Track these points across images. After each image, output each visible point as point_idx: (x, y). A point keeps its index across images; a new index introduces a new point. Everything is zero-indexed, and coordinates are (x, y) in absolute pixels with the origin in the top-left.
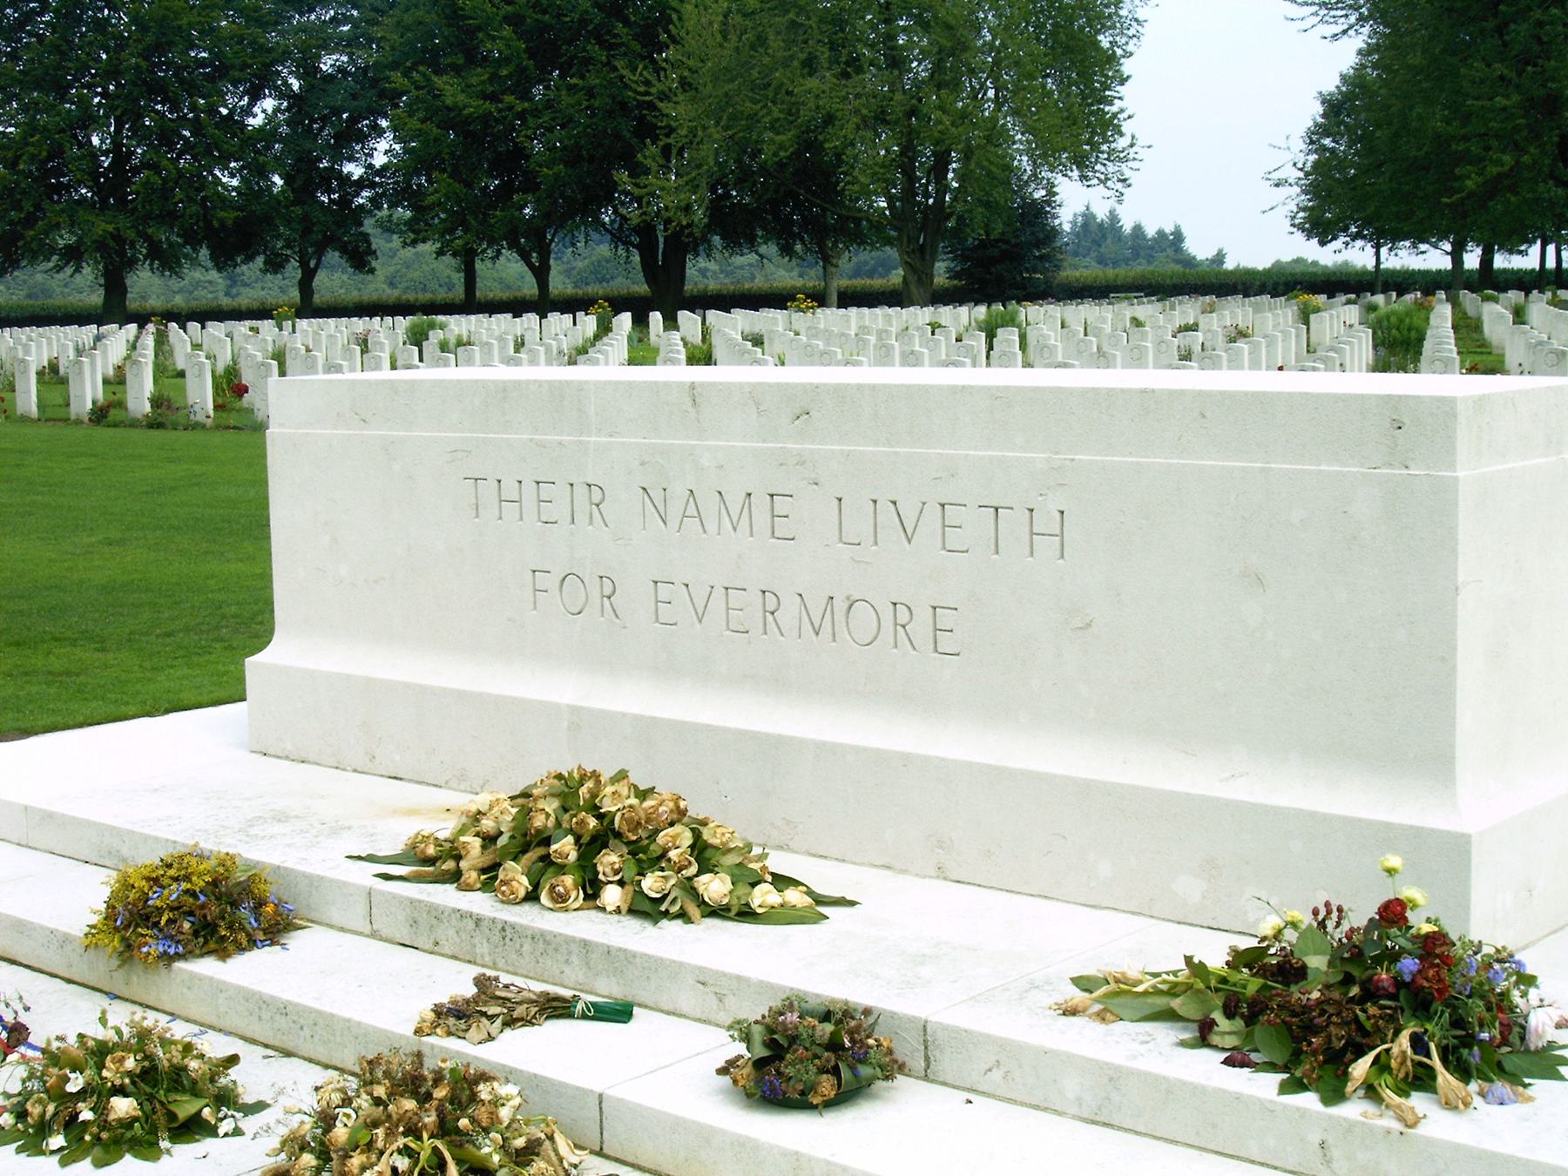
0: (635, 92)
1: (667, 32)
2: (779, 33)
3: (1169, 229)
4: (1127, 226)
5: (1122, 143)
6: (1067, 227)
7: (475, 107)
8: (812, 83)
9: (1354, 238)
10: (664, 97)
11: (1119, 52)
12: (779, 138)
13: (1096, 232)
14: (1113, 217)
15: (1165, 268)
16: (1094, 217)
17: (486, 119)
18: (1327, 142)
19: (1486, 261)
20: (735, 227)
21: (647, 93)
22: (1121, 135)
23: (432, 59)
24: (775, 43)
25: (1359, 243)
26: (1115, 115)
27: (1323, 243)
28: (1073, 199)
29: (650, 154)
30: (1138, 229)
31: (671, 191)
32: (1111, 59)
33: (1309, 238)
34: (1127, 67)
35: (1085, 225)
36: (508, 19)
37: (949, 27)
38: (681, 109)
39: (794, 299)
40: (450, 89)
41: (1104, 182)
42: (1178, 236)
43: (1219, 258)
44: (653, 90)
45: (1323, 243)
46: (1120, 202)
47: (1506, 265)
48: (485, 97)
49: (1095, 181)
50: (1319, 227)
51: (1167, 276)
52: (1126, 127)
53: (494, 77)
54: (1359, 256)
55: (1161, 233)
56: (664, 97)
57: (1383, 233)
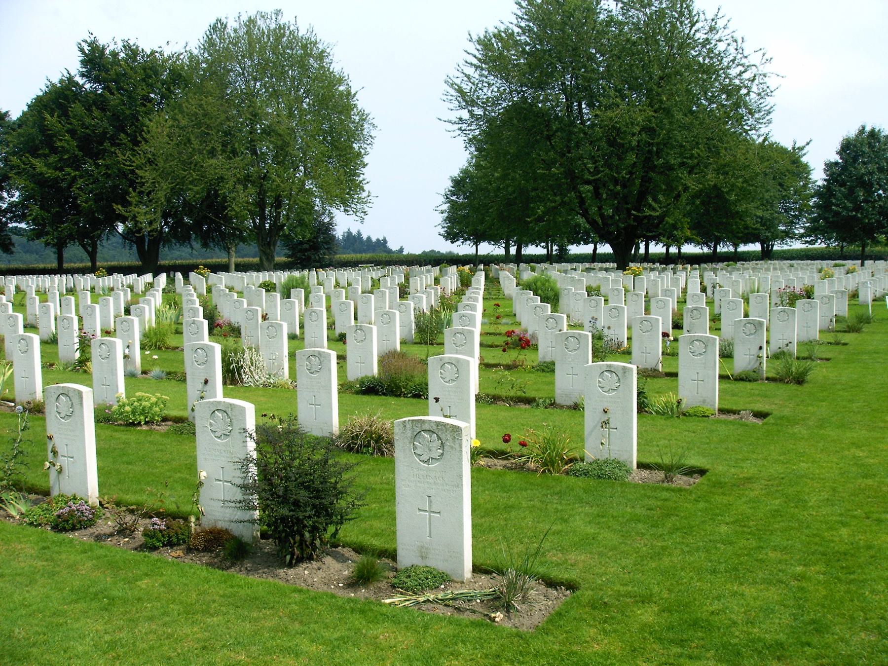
0: (124, 164)
1: (141, 135)
2: (197, 137)
3: (381, 238)
4: (365, 237)
5: (364, 194)
6: (341, 238)
7: (49, 173)
8: (213, 161)
9: (466, 240)
10: (139, 167)
11: (363, 151)
12: (196, 189)
13: (353, 240)
14: (359, 233)
15: (383, 256)
16: (351, 233)
17: (56, 180)
18: (454, 198)
19: (519, 250)
20: (181, 234)
21: (131, 166)
22: (364, 191)
23: (34, 152)
24: (196, 143)
25: (468, 242)
26: (361, 182)
27: (452, 242)
28: (343, 223)
29: (133, 197)
30: (369, 238)
31: (146, 216)
32: (359, 155)
33: (447, 240)
34: (366, 159)
35: (348, 236)
36: (68, 131)
37: (280, 135)
38: (147, 174)
39: (198, 268)
40: (39, 165)
41: (355, 212)
42: (385, 241)
43: (401, 250)
44: (134, 164)
45: (452, 242)
46: (362, 222)
47: (779, 249)
48: (56, 169)
49: (351, 212)
50: (451, 236)
51: (378, 256)
52: (366, 187)
53: (61, 159)
54: (464, 248)
55: (378, 240)
56: (139, 167)
57: (478, 239)
